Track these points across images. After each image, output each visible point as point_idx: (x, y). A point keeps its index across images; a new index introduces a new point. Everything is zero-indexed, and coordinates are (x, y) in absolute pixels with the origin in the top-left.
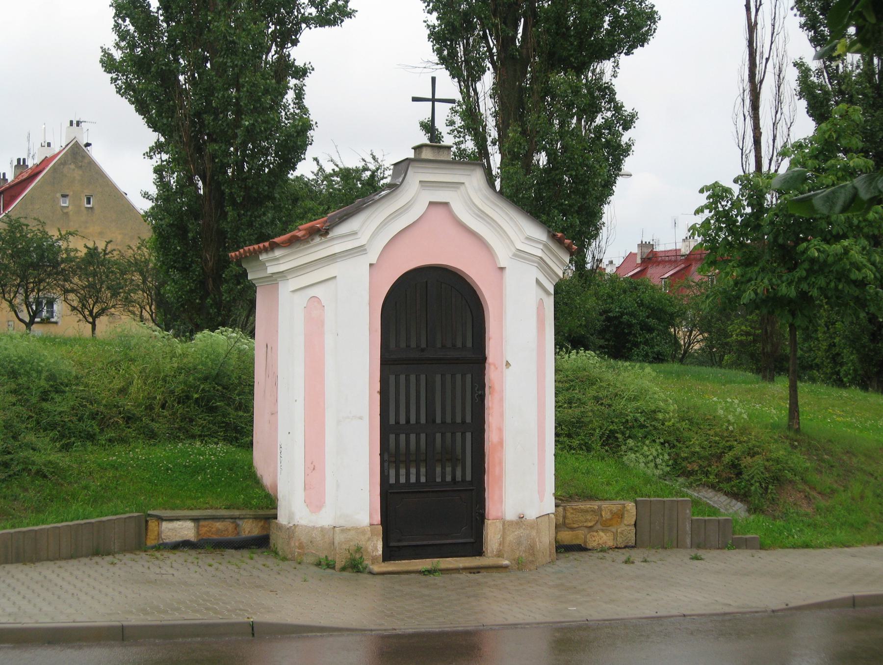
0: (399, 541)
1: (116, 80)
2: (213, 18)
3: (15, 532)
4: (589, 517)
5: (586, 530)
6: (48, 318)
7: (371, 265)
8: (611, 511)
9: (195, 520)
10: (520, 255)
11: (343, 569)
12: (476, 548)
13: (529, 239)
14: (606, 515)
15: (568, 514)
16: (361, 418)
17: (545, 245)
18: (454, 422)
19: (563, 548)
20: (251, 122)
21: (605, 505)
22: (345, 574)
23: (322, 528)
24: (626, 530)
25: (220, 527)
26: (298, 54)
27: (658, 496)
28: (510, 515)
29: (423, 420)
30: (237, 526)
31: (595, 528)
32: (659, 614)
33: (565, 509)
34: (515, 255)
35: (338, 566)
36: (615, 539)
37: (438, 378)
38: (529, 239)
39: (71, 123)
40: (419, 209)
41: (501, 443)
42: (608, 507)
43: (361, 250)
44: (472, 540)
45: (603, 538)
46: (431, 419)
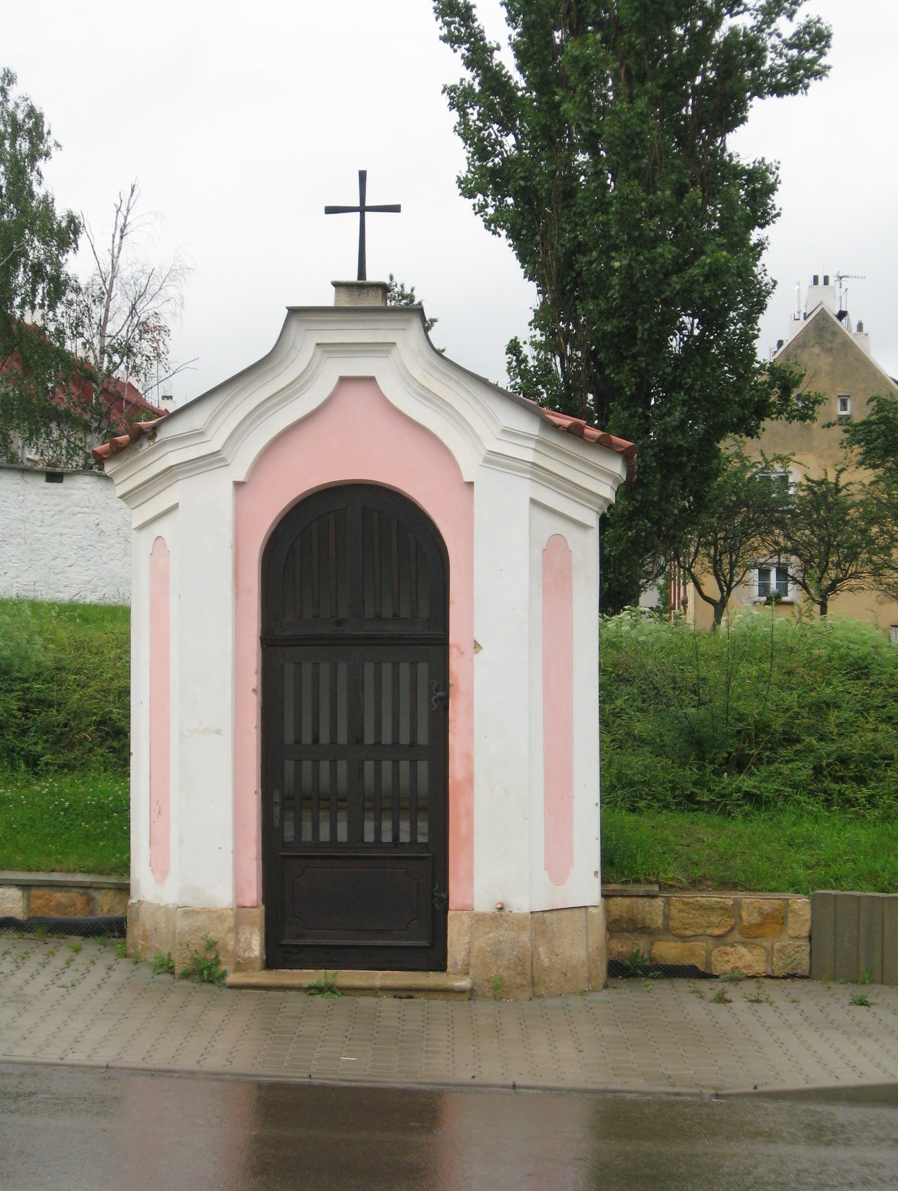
0: (299, 936)
1: (482, 208)
2: (563, 98)
4: (715, 919)
5: (711, 942)
6: (778, 596)
7: (238, 485)
8: (760, 911)
9: (24, 886)
10: (494, 459)
11: (186, 975)
12: (434, 956)
13: (507, 432)
14: (749, 916)
15: (674, 912)
16: (218, 732)
17: (539, 442)
18: (396, 743)
19: (620, 970)
20: (625, 262)
21: (747, 899)
22: (184, 982)
23: (166, 907)
24: (792, 943)
25: (62, 900)
26: (743, 145)
28: (483, 903)
29: (342, 739)
30: (90, 900)
31: (729, 939)
32: (477, 1080)
33: (667, 903)
34: (487, 460)
35: (178, 970)
36: (769, 960)
37: (369, 669)
38: (507, 432)
39: (816, 280)
41: (470, 780)
42: (753, 905)
43: (213, 460)
44: (425, 943)
45: (745, 957)
46: (357, 738)
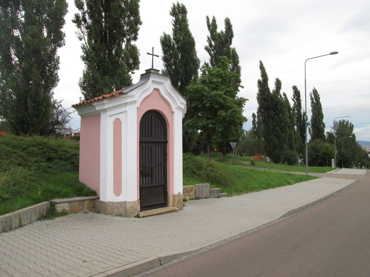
3: (72, 197)
10: (179, 108)
27: (288, 174)
40: (151, 90)
43: (135, 102)
